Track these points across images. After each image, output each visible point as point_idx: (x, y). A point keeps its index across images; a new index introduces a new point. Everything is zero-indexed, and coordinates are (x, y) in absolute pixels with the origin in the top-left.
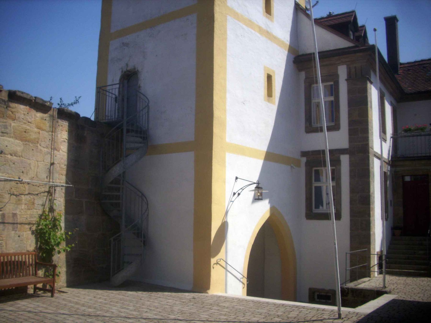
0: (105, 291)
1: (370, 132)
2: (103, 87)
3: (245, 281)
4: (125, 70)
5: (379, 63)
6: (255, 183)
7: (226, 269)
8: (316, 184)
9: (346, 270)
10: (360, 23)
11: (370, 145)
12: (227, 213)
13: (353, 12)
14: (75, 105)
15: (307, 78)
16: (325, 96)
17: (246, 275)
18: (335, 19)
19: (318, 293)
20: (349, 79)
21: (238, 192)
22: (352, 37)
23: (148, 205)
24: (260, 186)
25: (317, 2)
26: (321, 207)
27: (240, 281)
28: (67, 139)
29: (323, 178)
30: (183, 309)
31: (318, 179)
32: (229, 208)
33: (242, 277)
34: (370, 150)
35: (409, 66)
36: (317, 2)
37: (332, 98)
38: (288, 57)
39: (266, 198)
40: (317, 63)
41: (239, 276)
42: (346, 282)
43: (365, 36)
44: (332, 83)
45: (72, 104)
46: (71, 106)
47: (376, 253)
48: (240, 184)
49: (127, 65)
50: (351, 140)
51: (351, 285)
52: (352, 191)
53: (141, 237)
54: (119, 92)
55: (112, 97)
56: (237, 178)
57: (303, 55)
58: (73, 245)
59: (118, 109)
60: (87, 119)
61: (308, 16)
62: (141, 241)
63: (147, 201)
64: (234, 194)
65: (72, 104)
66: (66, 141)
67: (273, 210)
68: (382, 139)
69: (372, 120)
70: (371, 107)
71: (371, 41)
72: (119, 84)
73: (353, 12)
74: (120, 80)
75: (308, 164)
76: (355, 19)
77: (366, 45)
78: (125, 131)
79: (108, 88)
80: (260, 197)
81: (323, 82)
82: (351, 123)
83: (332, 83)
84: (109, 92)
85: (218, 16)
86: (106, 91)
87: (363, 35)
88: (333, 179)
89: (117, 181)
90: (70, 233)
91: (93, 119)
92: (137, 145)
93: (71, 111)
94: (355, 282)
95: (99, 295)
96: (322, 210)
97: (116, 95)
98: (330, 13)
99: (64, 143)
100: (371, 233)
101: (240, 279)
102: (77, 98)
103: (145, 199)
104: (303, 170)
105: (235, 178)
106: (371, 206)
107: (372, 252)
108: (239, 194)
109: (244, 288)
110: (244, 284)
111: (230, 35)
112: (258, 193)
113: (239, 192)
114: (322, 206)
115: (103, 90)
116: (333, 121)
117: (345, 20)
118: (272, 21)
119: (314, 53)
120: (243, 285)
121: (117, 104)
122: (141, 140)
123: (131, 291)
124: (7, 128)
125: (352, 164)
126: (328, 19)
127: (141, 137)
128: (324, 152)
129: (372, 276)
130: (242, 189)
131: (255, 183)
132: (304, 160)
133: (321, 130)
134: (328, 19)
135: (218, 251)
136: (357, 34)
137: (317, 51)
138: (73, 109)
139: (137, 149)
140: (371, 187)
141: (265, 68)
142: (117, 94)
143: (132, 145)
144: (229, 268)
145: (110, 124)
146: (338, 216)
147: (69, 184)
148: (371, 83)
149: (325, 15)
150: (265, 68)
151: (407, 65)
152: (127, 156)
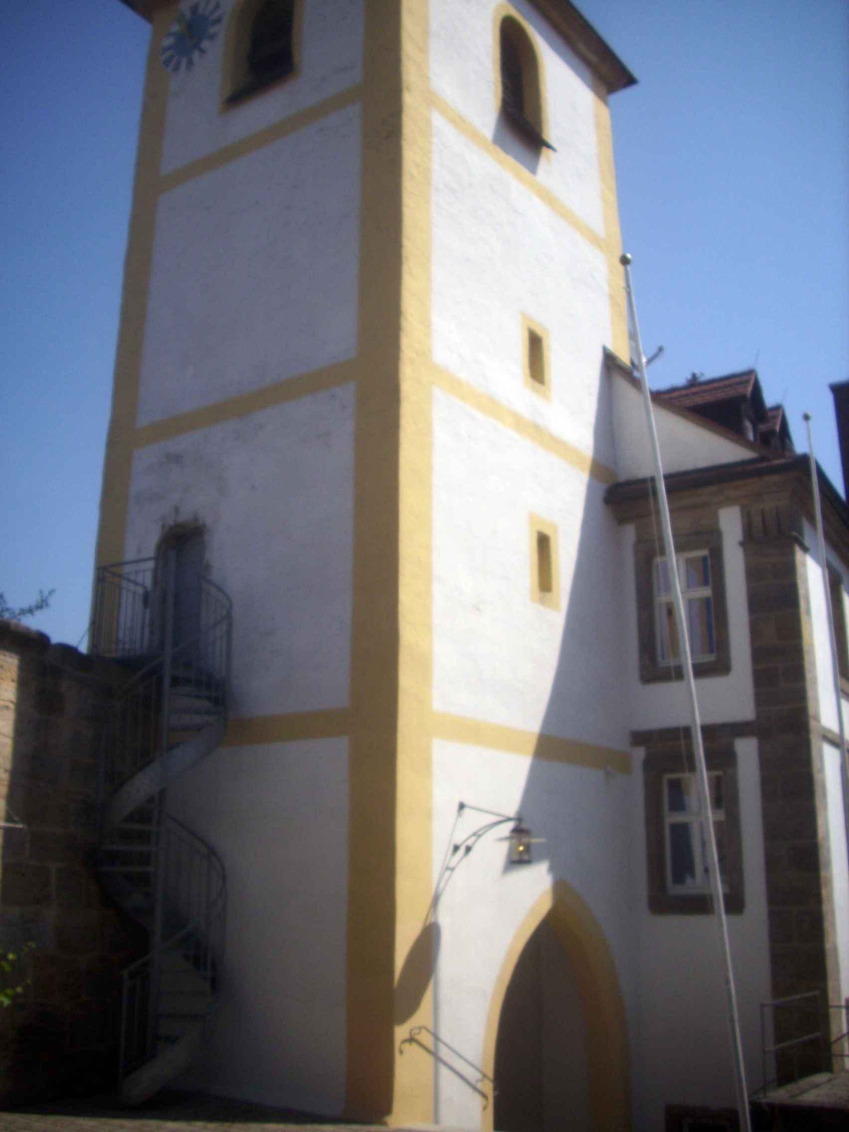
0: (103, 1120)
1: (808, 676)
2: (113, 566)
3: (488, 1087)
4: (170, 522)
5: (822, 501)
6: (509, 819)
7: (435, 1054)
8: (671, 818)
10: (770, 399)
11: (811, 711)
12: (435, 901)
13: (751, 373)
14: (38, 613)
15: (639, 541)
16: (689, 584)
17: (490, 1071)
18: (705, 391)
20: (749, 540)
22: (751, 436)
23: (224, 878)
24: (525, 826)
25: (661, 349)
26: (689, 881)
27: (475, 1089)
28: (12, 702)
29: (692, 801)
31: (678, 804)
32: (442, 885)
34: (813, 724)
37: (706, 592)
38: (590, 489)
39: (540, 858)
40: (660, 502)
41: (472, 1074)
42: (764, 1089)
43: (784, 433)
44: (704, 552)
45: (30, 611)
46: (29, 615)
47: (843, 1003)
48: (473, 821)
49: (177, 510)
50: (760, 699)
51: (780, 1095)
52: (772, 833)
54: (155, 582)
55: (135, 593)
56: (462, 806)
57: (629, 483)
58: (19, 990)
59: (152, 625)
60: (68, 651)
61: (636, 383)
63: (223, 869)
64: (456, 848)
65: (30, 611)
66: (12, 706)
67: (560, 889)
68: (841, 694)
69: (812, 645)
70: (808, 612)
71: (800, 446)
72: (156, 559)
73: (751, 373)
74: (159, 548)
75: (649, 764)
76: (757, 389)
77: (787, 454)
78: (167, 681)
79: (127, 569)
80: (526, 857)
81: (679, 548)
82: (759, 654)
83: (704, 552)
84: (129, 580)
85: (408, 387)
86: (120, 576)
87: (778, 428)
88: (718, 802)
89: (142, 815)
90: (11, 956)
91: (84, 648)
92: (197, 719)
93: (28, 629)
94: (791, 1088)
96: (692, 886)
97: (145, 587)
98: (694, 376)
99: (6, 712)
100: (828, 946)
101: (473, 1081)
102: (46, 593)
104: (638, 777)
105: (456, 807)
106: (823, 874)
107: (832, 1000)
108: (468, 849)
109: (485, 1108)
110: (484, 1096)
111: (441, 435)
112: (520, 845)
113: (469, 843)
114: (693, 876)
115: (114, 574)
116: (711, 651)
117: (731, 393)
118: (546, 397)
119: (653, 479)
120: (485, 1102)
121: (148, 611)
122: (206, 704)
123: (175, 1119)
125: (765, 762)
126: (688, 391)
127: (208, 698)
128: (687, 732)
129: (836, 1067)
131: (509, 819)
132: (639, 754)
133: (678, 674)
134: (688, 391)
135: (412, 1005)
136: (763, 427)
137: (662, 474)
138: (34, 623)
139: (199, 728)
140: (820, 821)
141: (533, 518)
142: (149, 583)
144: (444, 1053)
146: (735, 904)
147: (15, 822)
148: (805, 549)
149: (679, 379)
150: (533, 518)
152: (171, 748)
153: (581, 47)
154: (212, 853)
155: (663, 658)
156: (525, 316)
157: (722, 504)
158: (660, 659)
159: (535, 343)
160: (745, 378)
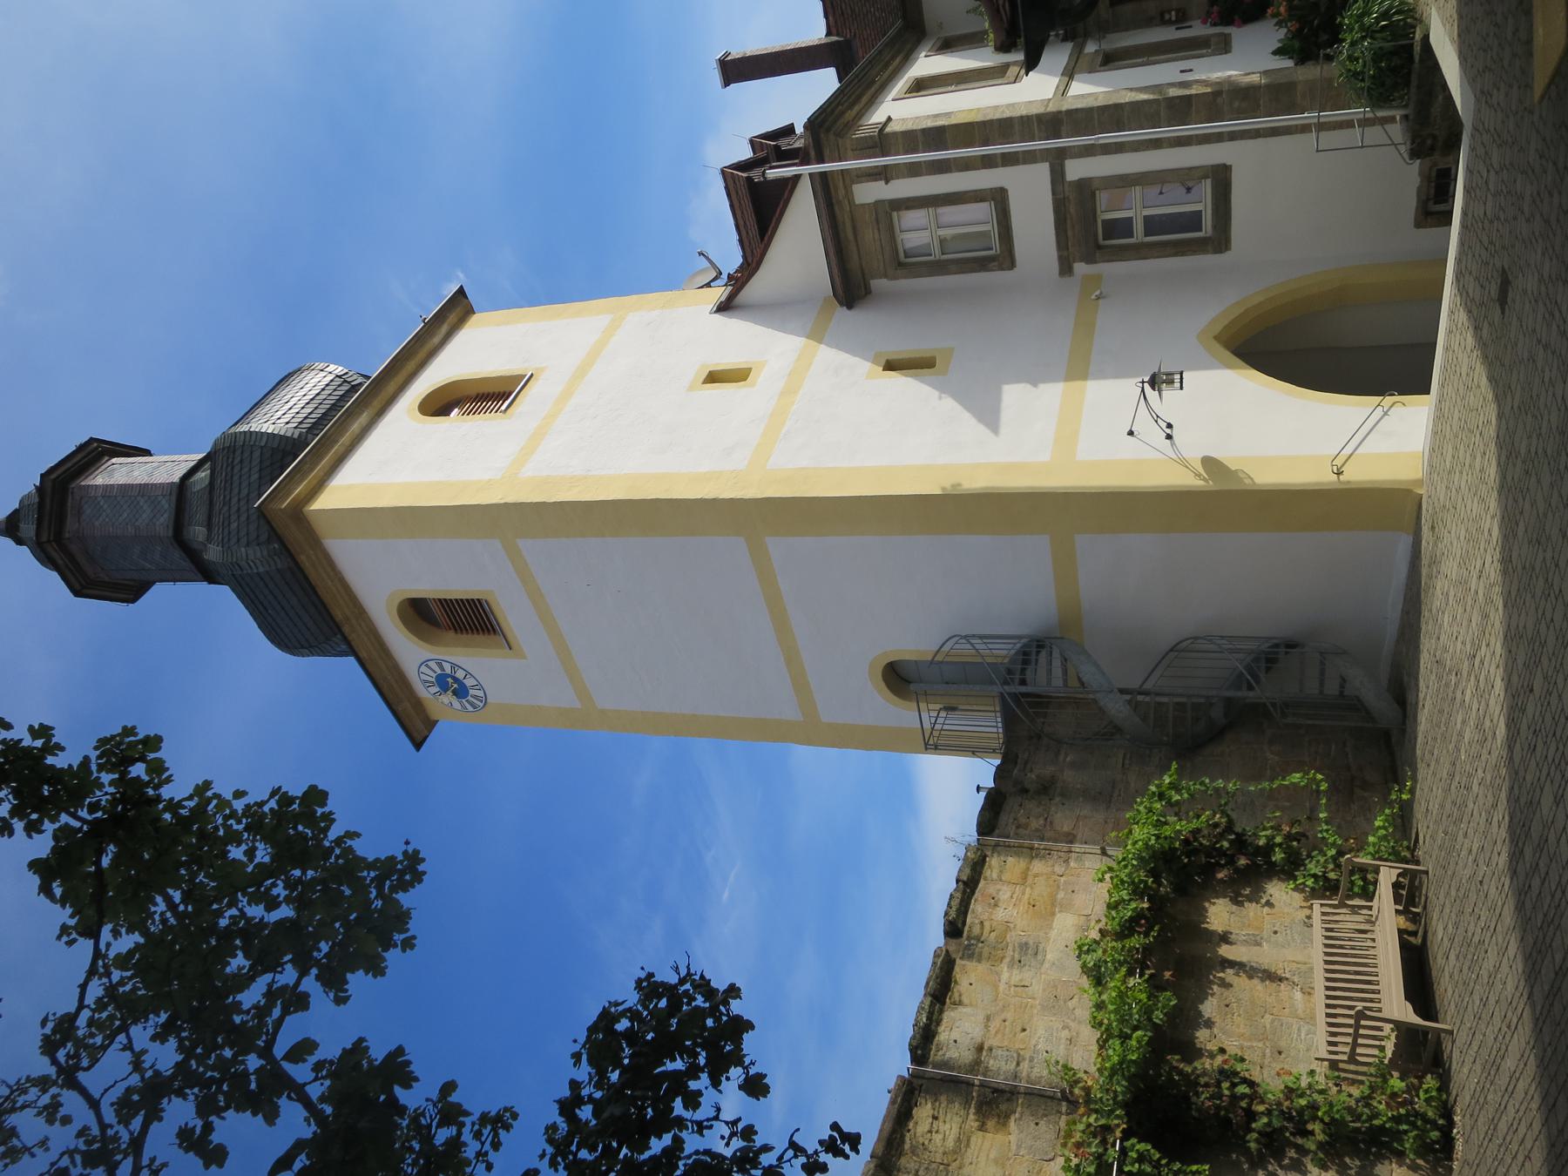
9: (1362, 147)
19: (1431, 202)
21: (1164, 427)
23: (1196, 638)
25: (701, 254)
30: (1458, 556)
33: (1380, 408)
34: (1051, 108)
35: (834, 13)
36: (701, 254)
48: (1144, 424)
53: (1277, 653)
56: (1131, 433)
60: (1000, 774)
62: (1287, 653)
75: (1090, 260)
78: (1023, 689)
91: (997, 762)
92: (1057, 663)
95: (1207, 1098)
103: (1185, 644)
108: (1170, 426)
113: (1164, 425)
122: (1043, 653)
124: (1026, 944)
127: (1038, 653)
130: (1157, 418)
132: (1080, 268)
143: (1057, 671)
145: (1010, 722)
151: (831, 18)
153: (436, 340)
154: (1176, 650)
155: (991, 249)
156: (691, 388)
157: (851, 201)
158: (992, 252)
159: (713, 378)
160: (730, 180)
